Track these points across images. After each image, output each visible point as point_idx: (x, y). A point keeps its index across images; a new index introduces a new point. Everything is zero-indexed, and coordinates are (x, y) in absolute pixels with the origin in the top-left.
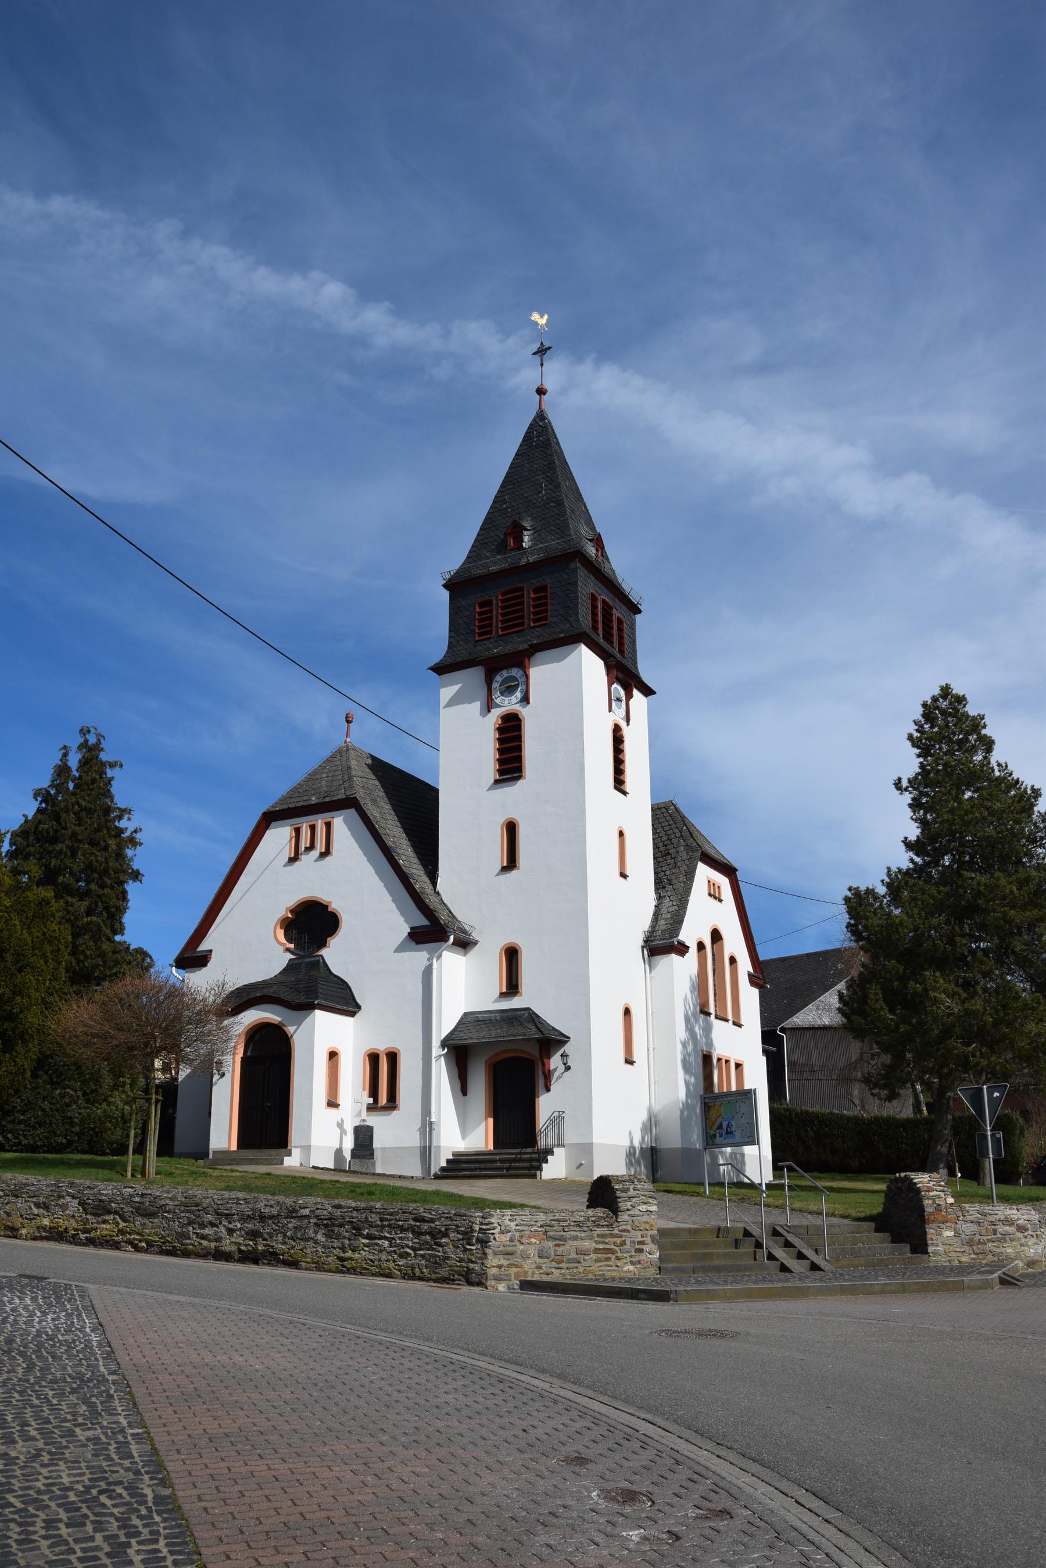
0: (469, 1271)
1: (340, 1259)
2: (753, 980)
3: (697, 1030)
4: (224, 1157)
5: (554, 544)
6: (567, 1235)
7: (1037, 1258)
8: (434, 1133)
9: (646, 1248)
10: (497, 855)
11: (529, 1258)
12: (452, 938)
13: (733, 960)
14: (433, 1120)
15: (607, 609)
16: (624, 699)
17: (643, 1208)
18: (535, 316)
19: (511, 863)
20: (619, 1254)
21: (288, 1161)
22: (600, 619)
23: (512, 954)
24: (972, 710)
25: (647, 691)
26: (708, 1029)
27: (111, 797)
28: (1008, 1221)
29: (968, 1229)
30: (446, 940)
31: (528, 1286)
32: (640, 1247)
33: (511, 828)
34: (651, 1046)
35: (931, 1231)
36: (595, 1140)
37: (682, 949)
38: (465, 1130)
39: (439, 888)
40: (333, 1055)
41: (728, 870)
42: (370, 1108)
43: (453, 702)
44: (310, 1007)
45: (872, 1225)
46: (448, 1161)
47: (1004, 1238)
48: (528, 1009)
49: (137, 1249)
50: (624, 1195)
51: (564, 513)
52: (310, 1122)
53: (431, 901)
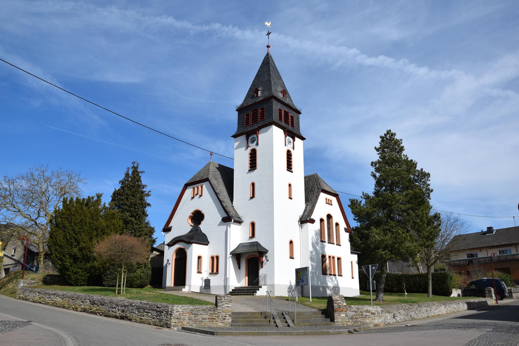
0: (167, 324)
1: (141, 319)
2: (346, 230)
4: (170, 289)
5: (267, 94)
10: (249, 194)
11: (185, 320)
13: (337, 224)
15: (286, 113)
17: (226, 305)
18: (266, 23)
19: (253, 197)
21: (184, 290)
23: (253, 224)
24: (397, 137)
25: (303, 138)
26: (323, 247)
27: (141, 182)
28: (367, 311)
29: (350, 314)
31: (184, 329)
33: (253, 185)
35: (336, 315)
36: (276, 283)
37: (312, 221)
38: (239, 281)
39: (233, 205)
41: (336, 195)
42: (210, 274)
43: (238, 148)
44: (192, 243)
45: (321, 312)
46: (233, 290)
47: (366, 317)
49: (100, 315)
51: (271, 84)
53: (229, 209)
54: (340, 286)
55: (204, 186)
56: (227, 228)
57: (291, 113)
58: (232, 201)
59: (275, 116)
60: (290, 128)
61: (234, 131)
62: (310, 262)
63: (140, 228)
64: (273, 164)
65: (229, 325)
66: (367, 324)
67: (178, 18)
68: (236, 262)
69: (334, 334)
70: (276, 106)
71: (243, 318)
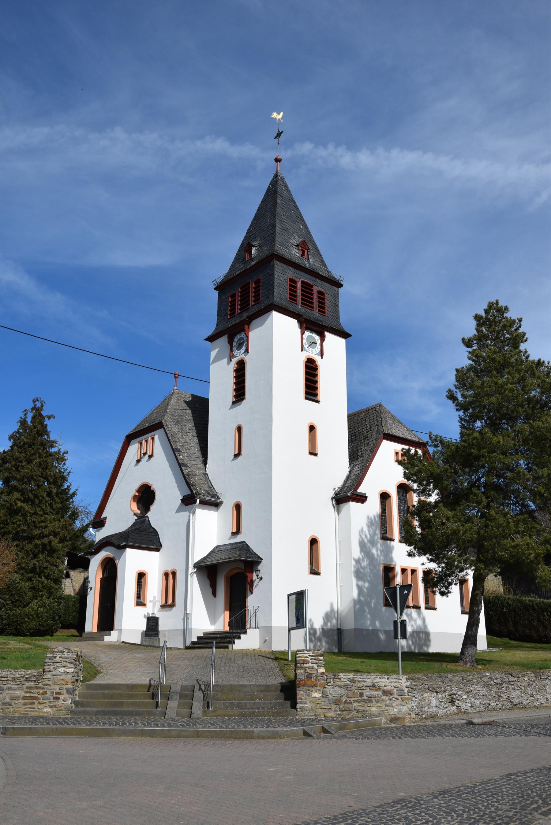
3: (374, 551)
5: (266, 252)
6: (5, 687)
7: (400, 716)
8: (189, 621)
9: (62, 697)
12: (198, 501)
14: (188, 612)
15: (307, 287)
16: (319, 342)
17: (62, 670)
18: (275, 115)
19: (237, 456)
20: (41, 701)
22: (252, 294)
23: (238, 507)
24: (511, 315)
26: (388, 551)
28: (374, 687)
29: (333, 691)
30: (195, 502)
32: (58, 696)
33: (239, 429)
34: (338, 562)
36: (273, 624)
37: (362, 499)
38: (213, 619)
39: (208, 471)
40: (141, 576)
42: (162, 606)
44: (125, 547)
46: (199, 638)
47: (370, 699)
48: (244, 542)
50: (50, 661)
51: (275, 232)
52: (122, 615)
54: (431, 629)
55: (156, 438)
56: (189, 516)
57: (318, 286)
58: (205, 463)
59: (281, 292)
60: (315, 314)
61: (210, 330)
62: (354, 581)
63: (42, 522)
64: (272, 387)
65: (64, 712)
66: (371, 715)
67: (234, 140)
68: (208, 582)
69: (264, 738)
70: (282, 275)
71: (105, 696)
